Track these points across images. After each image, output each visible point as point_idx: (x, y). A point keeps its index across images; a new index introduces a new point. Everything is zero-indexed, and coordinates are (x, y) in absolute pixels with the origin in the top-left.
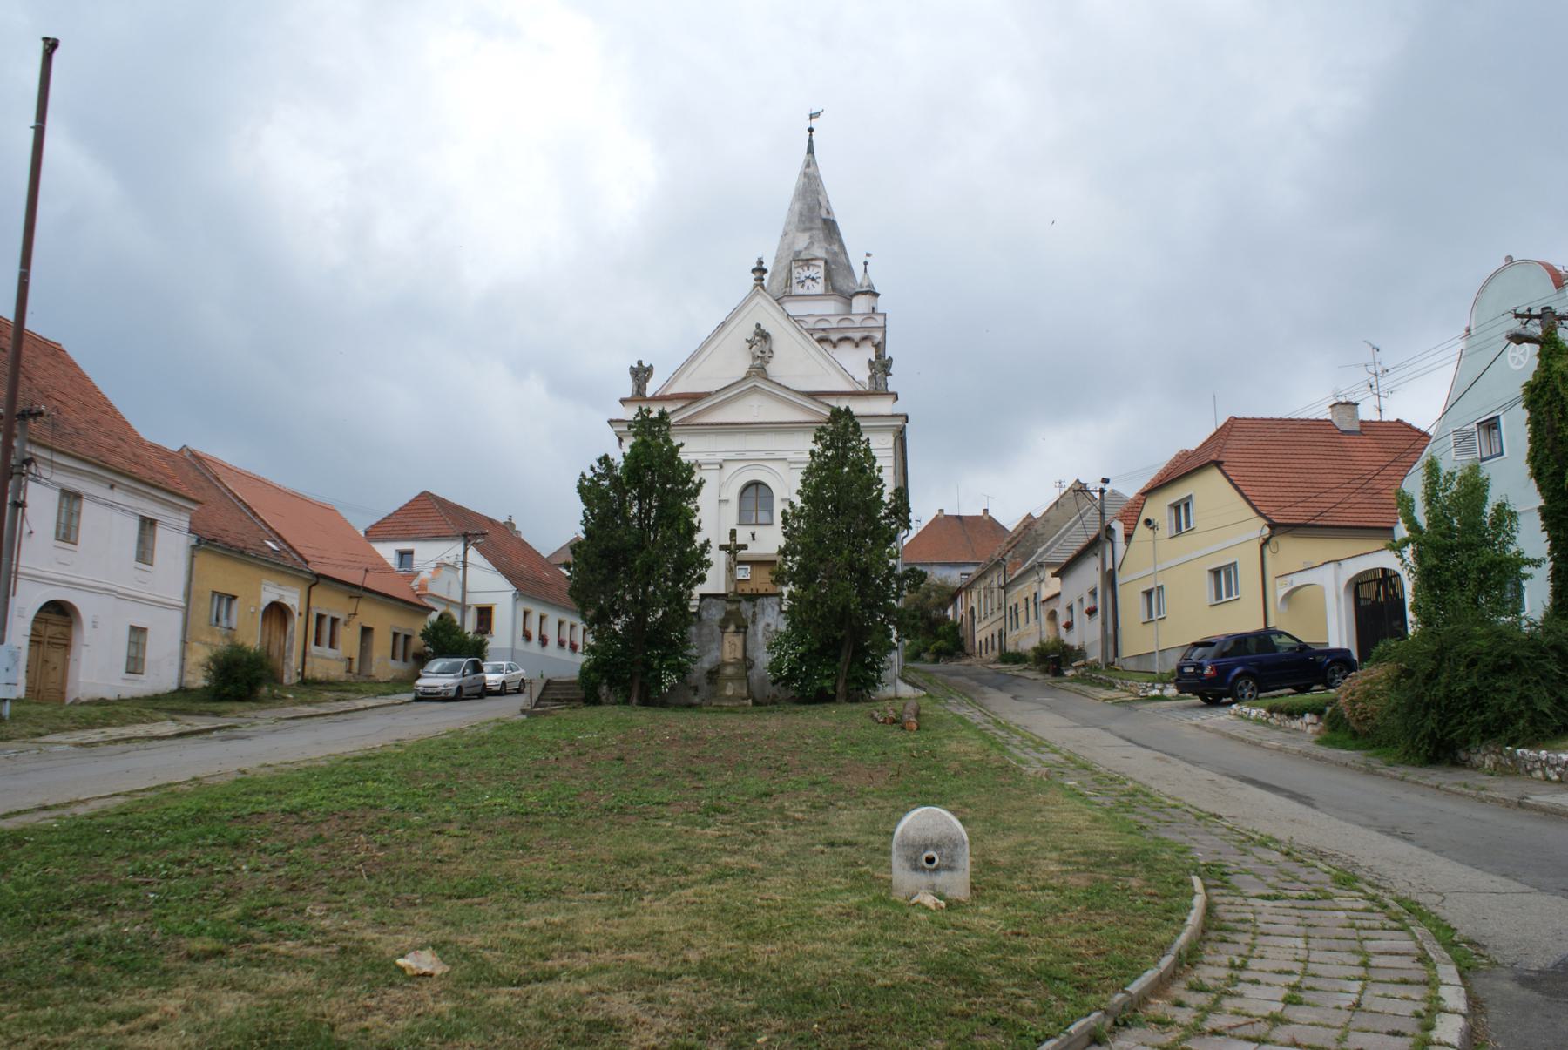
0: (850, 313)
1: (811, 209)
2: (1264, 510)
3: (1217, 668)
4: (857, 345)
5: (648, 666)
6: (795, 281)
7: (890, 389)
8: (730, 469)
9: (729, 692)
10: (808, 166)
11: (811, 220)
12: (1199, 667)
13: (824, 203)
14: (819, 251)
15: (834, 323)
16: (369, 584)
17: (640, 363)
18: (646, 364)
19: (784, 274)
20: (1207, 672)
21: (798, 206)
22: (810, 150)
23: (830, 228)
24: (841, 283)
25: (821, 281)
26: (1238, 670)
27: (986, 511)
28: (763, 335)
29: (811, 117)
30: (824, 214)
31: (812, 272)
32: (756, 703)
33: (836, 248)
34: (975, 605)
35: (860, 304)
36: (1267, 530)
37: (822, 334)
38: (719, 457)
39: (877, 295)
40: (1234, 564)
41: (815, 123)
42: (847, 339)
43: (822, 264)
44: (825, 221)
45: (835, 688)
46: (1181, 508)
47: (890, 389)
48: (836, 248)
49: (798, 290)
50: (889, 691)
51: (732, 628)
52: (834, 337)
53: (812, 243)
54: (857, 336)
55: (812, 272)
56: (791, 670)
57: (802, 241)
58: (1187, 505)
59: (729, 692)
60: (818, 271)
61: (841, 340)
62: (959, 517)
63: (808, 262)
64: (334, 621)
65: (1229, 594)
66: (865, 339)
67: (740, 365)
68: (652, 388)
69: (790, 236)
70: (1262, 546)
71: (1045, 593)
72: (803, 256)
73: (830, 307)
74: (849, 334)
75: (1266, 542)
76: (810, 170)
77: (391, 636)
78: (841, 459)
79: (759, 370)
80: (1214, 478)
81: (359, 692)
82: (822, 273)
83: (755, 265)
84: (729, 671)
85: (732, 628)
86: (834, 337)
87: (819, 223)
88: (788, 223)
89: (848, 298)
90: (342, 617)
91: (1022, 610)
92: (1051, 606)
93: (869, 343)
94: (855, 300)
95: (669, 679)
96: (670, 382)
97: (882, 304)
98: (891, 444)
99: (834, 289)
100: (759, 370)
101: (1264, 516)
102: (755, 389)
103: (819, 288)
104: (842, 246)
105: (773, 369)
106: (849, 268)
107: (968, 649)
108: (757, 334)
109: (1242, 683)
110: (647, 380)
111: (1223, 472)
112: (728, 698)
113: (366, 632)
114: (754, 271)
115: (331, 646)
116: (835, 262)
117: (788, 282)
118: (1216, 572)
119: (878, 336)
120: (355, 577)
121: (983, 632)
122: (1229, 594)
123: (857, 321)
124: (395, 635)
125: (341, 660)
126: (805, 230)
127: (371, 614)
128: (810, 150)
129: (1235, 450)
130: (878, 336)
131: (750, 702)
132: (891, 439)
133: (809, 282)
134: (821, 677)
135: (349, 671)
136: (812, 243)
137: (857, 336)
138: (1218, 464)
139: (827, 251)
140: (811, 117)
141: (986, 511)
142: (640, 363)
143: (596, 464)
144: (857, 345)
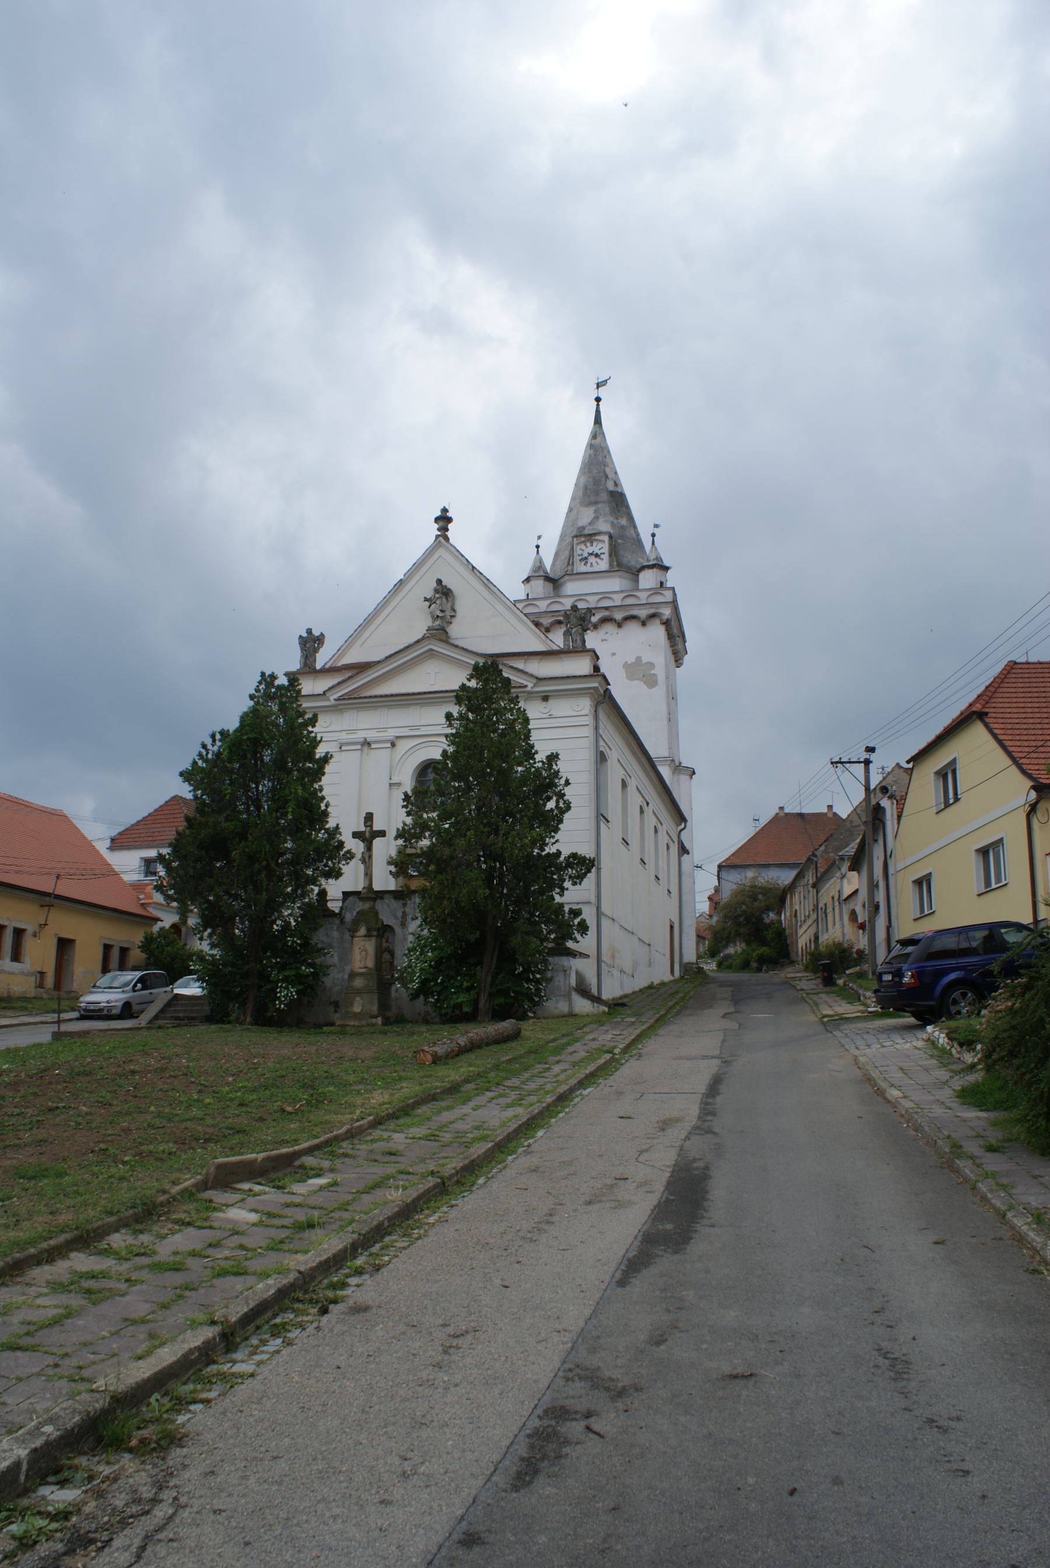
0: (637, 589)
1: (596, 482)
2: (1031, 768)
3: (918, 975)
4: (644, 624)
5: (264, 977)
6: (577, 558)
7: (588, 646)
8: (403, 746)
9: (357, 1009)
10: (594, 436)
11: (597, 493)
12: (898, 974)
13: (611, 475)
14: (604, 526)
15: (617, 600)
16: (61, 891)
17: (309, 631)
18: (316, 633)
19: (567, 553)
20: (906, 980)
21: (583, 479)
22: (598, 421)
23: (618, 501)
24: (630, 559)
25: (605, 557)
26: (953, 976)
27: (830, 807)
28: (443, 592)
29: (598, 386)
30: (611, 486)
31: (595, 548)
32: (387, 1021)
33: (623, 522)
34: (797, 907)
35: (648, 579)
36: (1033, 795)
37: (606, 613)
38: (391, 734)
39: (666, 569)
40: (1001, 840)
41: (602, 392)
42: (633, 617)
43: (606, 538)
44: (612, 494)
45: (475, 1003)
46: (947, 774)
47: (588, 646)
48: (623, 522)
49: (582, 568)
50: (563, 1007)
51: (363, 931)
52: (618, 616)
53: (597, 518)
54: (643, 613)
55: (595, 548)
56: (424, 982)
57: (586, 516)
58: (954, 772)
59: (357, 1009)
60: (602, 546)
61: (627, 618)
62: (801, 815)
63: (591, 538)
64: (19, 933)
65: (998, 880)
66: (653, 616)
67: (420, 625)
68: (322, 659)
69: (574, 512)
70: (1028, 815)
71: (847, 891)
72: (586, 532)
73: (615, 584)
74: (635, 612)
75: (1033, 808)
76: (598, 441)
77: (101, 948)
78: (488, 726)
79: (440, 632)
80: (978, 735)
81: (25, 1009)
82: (606, 549)
83: (439, 514)
84: (358, 983)
85: (363, 931)
86: (618, 616)
87: (604, 496)
88: (573, 499)
89: (634, 573)
90: (30, 928)
91: (829, 910)
92: (851, 905)
93: (657, 621)
94: (642, 575)
95: (286, 993)
96: (342, 651)
97: (672, 579)
98: (586, 711)
99: (619, 565)
100: (440, 632)
101: (1029, 776)
102: (431, 654)
103: (603, 565)
104: (631, 519)
105: (455, 630)
106: (639, 542)
107: (793, 957)
108: (436, 591)
109: (956, 995)
110: (316, 650)
111: (986, 725)
112: (356, 1016)
113: (64, 945)
114: (437, 520)
115: (16, 957)
116: (622, 537)
117: (570, 561)
118: (984, 852)
119: (667, 612)
120: (45, 884)
121: (803, 939)
122: (998, 880)
123: (643, 597)
124: (107, 948)
125: (32, 974)
126: (590, 504)
127: (64, 924)
128: (598, 421)
129: (573, 537)
130: (667, 612)
131: (379, 1020)
132: (585, 705)
133: (592, 559)
134: (460, 989)
135: (41, 986)
136: (597, 518)
137: (643, 613)
138: (981, 716)
139: (613, 524)
140: (598, 386)
141: (830, 807)
142: (309, 631)
143: (209, 742)
144: (644, 624)
